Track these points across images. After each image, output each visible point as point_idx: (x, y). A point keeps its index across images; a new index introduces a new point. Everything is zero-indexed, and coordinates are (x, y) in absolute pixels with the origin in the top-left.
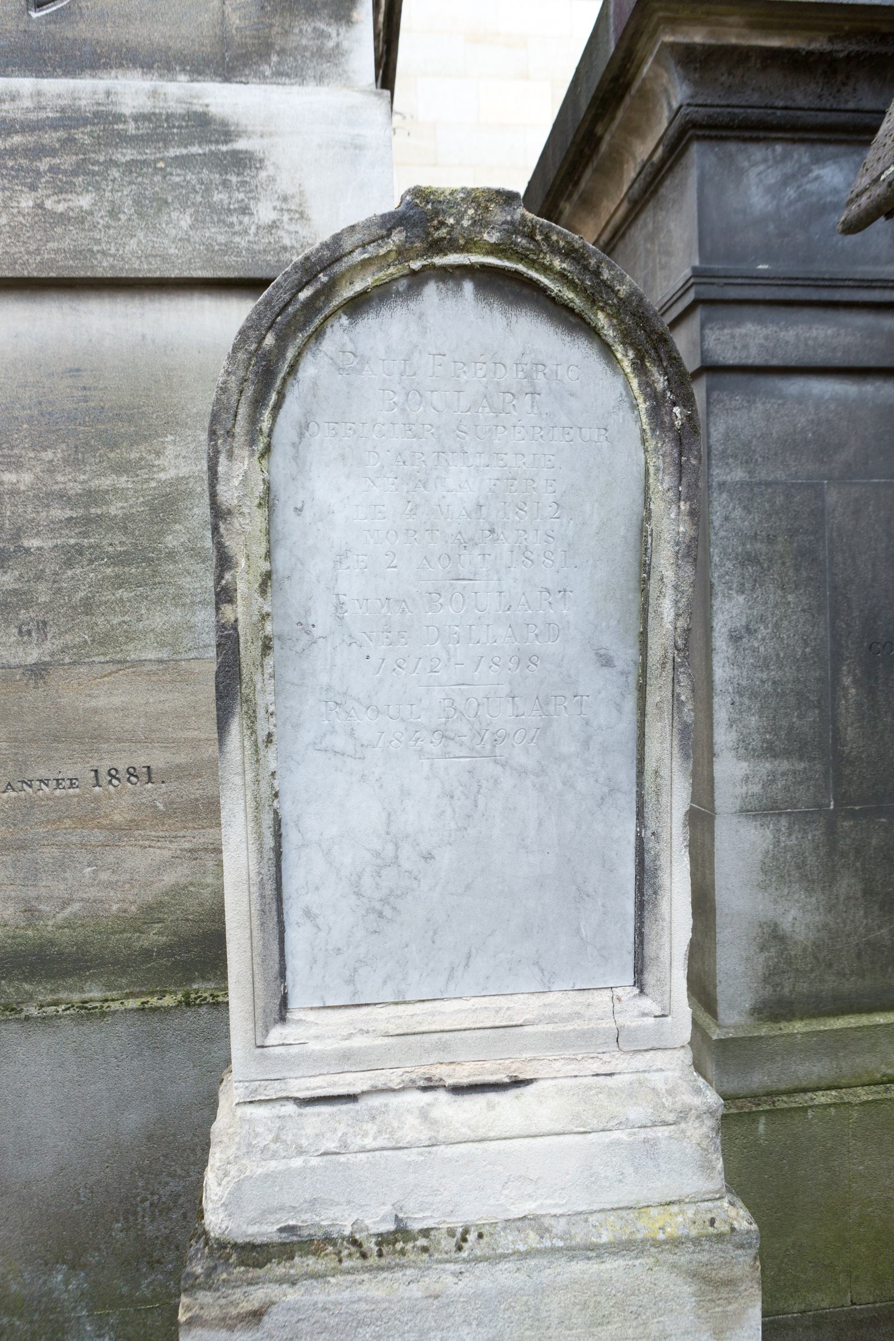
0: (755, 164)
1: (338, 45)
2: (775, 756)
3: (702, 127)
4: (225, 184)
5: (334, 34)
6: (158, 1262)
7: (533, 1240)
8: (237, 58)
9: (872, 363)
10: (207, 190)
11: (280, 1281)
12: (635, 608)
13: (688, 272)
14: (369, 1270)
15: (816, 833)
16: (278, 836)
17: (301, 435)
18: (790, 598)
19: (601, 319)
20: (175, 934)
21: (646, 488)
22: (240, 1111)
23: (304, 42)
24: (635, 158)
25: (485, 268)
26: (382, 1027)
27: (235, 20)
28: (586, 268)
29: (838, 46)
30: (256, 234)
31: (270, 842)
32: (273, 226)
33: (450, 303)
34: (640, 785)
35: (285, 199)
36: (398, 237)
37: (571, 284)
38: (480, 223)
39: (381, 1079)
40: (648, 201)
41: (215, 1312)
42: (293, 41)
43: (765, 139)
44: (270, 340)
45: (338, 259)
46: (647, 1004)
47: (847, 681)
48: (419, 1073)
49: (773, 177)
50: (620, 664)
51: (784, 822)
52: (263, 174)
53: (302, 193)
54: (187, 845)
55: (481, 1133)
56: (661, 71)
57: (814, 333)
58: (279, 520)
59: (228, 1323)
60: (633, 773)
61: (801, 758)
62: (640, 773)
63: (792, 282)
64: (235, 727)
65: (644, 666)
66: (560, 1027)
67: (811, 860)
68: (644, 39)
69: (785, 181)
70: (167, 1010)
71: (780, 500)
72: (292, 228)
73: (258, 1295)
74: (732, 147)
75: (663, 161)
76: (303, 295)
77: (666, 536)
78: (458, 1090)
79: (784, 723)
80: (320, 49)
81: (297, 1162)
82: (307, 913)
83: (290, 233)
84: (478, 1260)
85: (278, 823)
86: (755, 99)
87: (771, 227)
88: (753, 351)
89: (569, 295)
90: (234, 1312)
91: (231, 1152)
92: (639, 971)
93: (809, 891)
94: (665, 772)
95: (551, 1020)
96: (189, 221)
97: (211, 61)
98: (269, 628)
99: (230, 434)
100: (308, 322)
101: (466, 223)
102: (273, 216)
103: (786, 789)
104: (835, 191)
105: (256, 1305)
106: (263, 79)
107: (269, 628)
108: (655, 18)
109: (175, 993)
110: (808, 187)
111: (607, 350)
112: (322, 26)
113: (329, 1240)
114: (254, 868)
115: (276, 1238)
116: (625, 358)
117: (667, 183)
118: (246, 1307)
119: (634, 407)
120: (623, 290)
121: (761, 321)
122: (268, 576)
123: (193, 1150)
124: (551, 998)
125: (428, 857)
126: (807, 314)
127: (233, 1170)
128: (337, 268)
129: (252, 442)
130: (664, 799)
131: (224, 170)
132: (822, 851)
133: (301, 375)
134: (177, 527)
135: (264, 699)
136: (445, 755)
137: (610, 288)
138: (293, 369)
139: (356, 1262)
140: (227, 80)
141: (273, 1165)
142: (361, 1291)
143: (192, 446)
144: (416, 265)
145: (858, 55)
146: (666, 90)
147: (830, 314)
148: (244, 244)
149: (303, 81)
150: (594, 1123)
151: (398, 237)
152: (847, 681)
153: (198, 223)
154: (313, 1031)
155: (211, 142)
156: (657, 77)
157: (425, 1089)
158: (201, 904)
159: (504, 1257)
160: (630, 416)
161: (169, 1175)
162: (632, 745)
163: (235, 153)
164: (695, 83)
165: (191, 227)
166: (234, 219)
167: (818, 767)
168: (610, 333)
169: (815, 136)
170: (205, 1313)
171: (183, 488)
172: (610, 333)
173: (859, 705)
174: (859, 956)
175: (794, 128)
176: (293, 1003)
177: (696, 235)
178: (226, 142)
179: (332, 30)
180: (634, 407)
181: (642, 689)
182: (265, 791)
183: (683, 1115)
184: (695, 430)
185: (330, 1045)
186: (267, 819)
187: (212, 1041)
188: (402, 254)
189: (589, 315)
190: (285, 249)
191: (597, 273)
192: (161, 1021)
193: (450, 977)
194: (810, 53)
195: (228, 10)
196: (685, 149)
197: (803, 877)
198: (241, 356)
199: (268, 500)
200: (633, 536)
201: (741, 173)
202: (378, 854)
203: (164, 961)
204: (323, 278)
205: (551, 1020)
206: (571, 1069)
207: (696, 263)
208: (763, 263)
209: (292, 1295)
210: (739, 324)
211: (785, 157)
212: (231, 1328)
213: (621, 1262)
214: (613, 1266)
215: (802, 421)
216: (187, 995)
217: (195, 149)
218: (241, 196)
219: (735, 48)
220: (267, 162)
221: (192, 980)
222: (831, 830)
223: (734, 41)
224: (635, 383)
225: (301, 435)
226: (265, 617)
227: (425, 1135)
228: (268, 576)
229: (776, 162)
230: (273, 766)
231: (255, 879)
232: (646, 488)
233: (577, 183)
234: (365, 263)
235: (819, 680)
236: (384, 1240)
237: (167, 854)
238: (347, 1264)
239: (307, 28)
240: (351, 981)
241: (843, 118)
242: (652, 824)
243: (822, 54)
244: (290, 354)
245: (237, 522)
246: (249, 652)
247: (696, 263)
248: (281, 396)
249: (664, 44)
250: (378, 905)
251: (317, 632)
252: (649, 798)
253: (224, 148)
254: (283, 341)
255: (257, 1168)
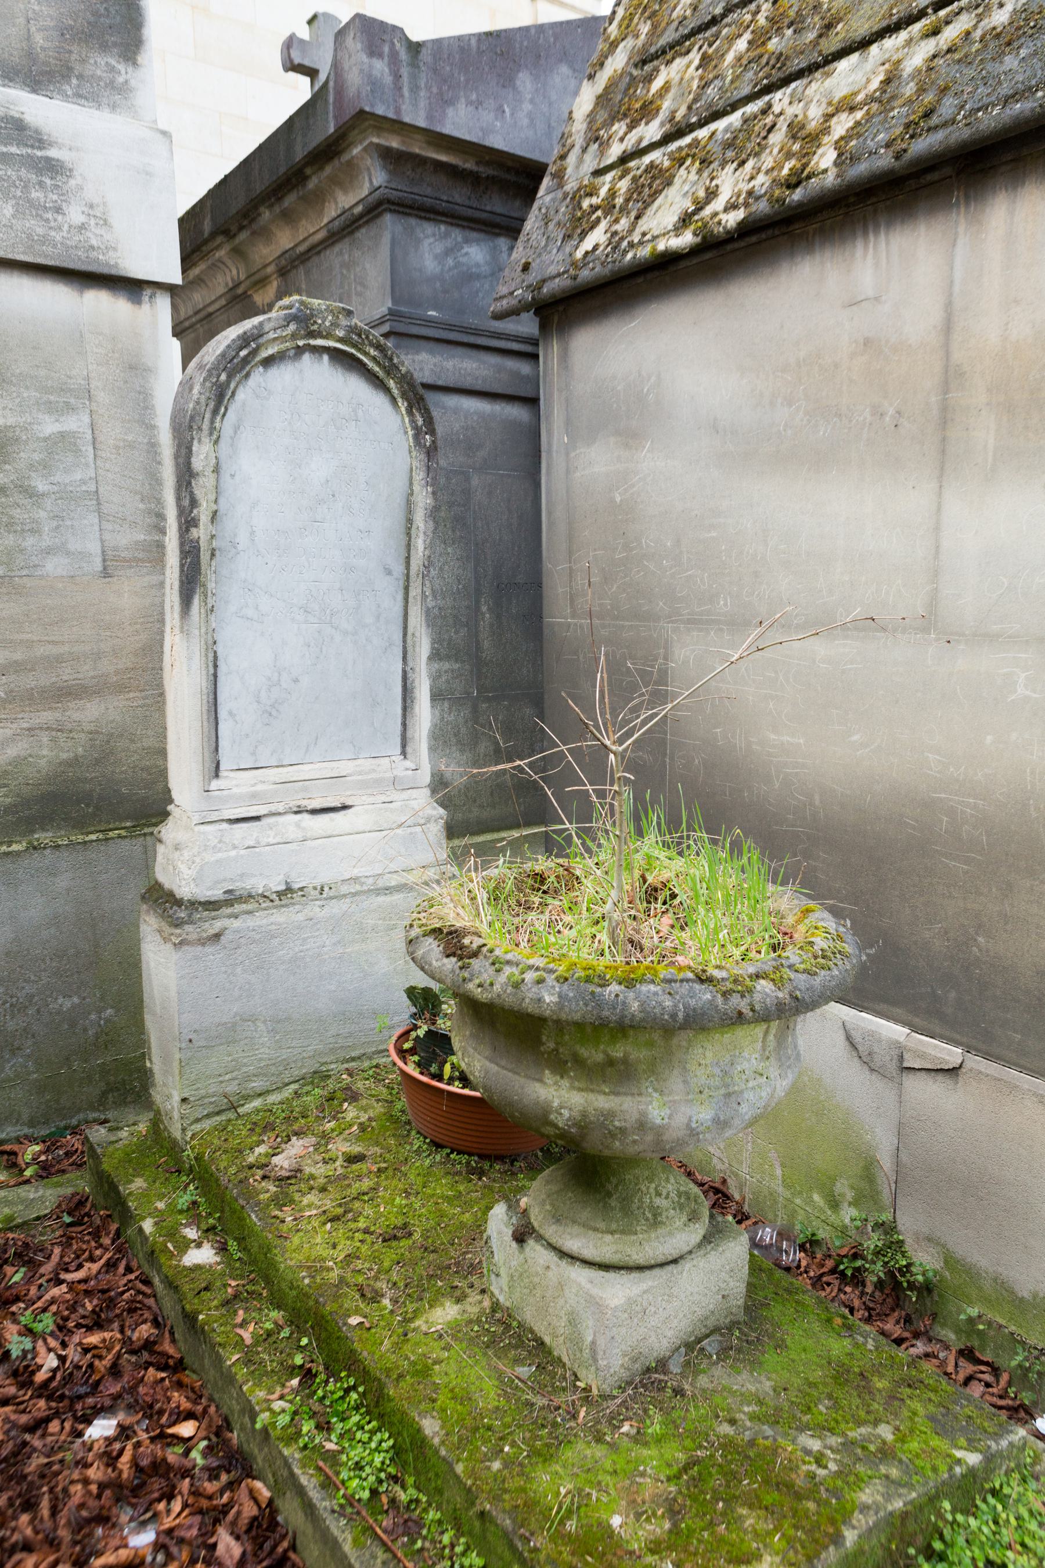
0: (427, 237)
1: (126, 81)
2: (440, 659)
3: (393, 203)
4: (41, 184)
5: (123, 71)
6: (18, 1049)
7: (358, 887)
8: (43, 73)
9: (500, 391)
10: (25, 187)
11: (229, 917)
12: (404, 543)
13: (384, 310)
14: (276, 907)
15: (466, 712)
16: (216, 666)
17: (235, 433)
18: (449, 550)
19: (392, 384)
20: (18, 795)
21: (411, 478)
22: (197, 828)
23: (99, 73)
24: (336, 203)
25: (336, 350)
26: (272, 779)
27: (39, 39)
28: (386, 356)
29: (481, 169)
30: (69, 232)
31: (212, 671)
32: (82, 227)
33: (316, 365)
34: (405, 641)
35: (91, 206)
36: (292, 327)
37: (378, 364)
38: (335, 325)
39: (273, 808)
40: (344, 237)
41: (195, 936)
42: (89, 70)
43: (434, 220)
44: (223, 377)
45: (261, 336)
46: (408, 764)
47: (484, 609)
48: (293, 804)
49: (439, 248)
50: (395, 573)
51: (446, 704)
52: (72, 182)
53: (104, 204)
54: (26, 725)
55: (329, 833)
56: (366, 156)
57: (465, 365)
58: (221, 481)
59: (202, 942)
60: (401, 635)
61: (456, 661)
62: (405, 635)
63: (451, 327)
64: (196, 601)
65: (408, 576)
66: (365, 777)
67: (463, 730)
68: (356, 131)
69: (448, 252)
70: (18, 853)
71: (443, 481)
72: (98, 231)
73: (218, 925)
74: (413, 221)
75: (361, 216)
76: (243, 353)
77: (421, 505)
78: (314, 812)
79: (446, 637)
80: (112, 82)
81: (233, 853)
82: (230, 713)
83: (96, 235)
84: (332, 898)
85: (216, 658)
86: (429, 191)
87: (438, 284)
88: (427, 373)
89: (377, 369)
90: (205, 935)
91: (195, 850)
92: (404, 746)
93: (462, 751)
94: (417, 634)
95: (360, 773)
96: (11, 211)
97: (19, 71)
98: (214, 544)
99: (200, 429)
100: (243, 368)
101: (327, 324)
102: (82, 219)
103: (447, 681)
104: (478, 265)
105: (217, 931)
106: (66, 98)
107: (214, 544)
108: (367, 123)
109: (20, 842)
110: (462, 259)
111: (394, 400)
112: (113, 62)
113: (250, 896)
114: (204, 684)
115: (222, 897)
116: (403, 405)
117: (363, 230)
118: (211, 932)
119: (406, 433)
120: (403, 370)
121: (431, 352)
122: (215, 513)
123: (43, 960)
124: (359, 762)
125: (296, 681)
126: (460, 350)
127: (197, 860)
128: (261, 341)
129: (211, 434)
130: (417, 649)
131: (40, 172)
132: (470, 724)
133: (236, 397)
134: (7, 467)
135: (211, 585)
136: (306, 622)
137: (397, 368)
138: (233, 393)
139: (268, 904)
140: (34, 91)
141: (220, 855)
142: (272, 919)
143: (17, 400)
144: (301, 343)
145: (493, 177)
146: (368, 169)
147: (474, 353)
148: (58, 238)
149: (99, 107)
150: (385, 826)
151: (292, 327)
152: (484, 609)
153: (18, 213)
154: (234, 782)
155: (27, 145)
156: (362, 158)
157: (296, 813)
158: (39, 772)
159: (344, 896)
160: (404, 438)
161: (25, 981)
162: (401, 619)
163: (48, 160)
164: (390, 172)
165: (14, 216)
166: (49, 216)
167: (467, 667)
168: (395, 392)
169: (465, 224)
170: (189, 937)
171: (11, 435)
172: (395, 392)
173: (491, 625)
174: (492, 794)
175: (453, 216)
176: (222, 767)
177: (389, 283)
178: (40, 148)
179: (121, 67)
180: (406, 433)
181: (407, 589)
182: (210, 642)
183: (428, 820)
184: (436, 448)
185: (244, 790)
186: (211, 655)
187: (55, 875)
188: (294, 336)
189: (386, 381)
190: (92, 247)
191: (391, 359)
192: (13, 863)
193: (307, 750)
194: (464, 170)
195: (33, 29)
196: (380, 215)
197: (459, 742)
198: (208, 384)
199: (217, 470)
200: (403, 503)
201: (419, 241)
202: (269, 679)
203: (10, 818)
204: (253, 345)
205: (360, 773)
206: (371, 799)
207: (390, 305)
208: (434, 309)
209: (236, 924)
210: (417, 353)
211: (446, 236)
212: (203, 944)
213: (402, 895)
214: (397, 897)
215: (457, 426)
216: (30, 843)
217: (13, 149)
218: (55, 197)
219: (417, 156)
220: (75, 173)
221: (33, 832)
222: (475, 710)
223: (417, 151)
224: (407, 420)
225: (235, 433)
226: (213, 537)
227: (300, 836)
228: (215, 513)
229: (441, 238)
230: (214, 625)
231: (205, 691)
232: (411, 478)
233: (280, 199)
234: (275, 339)
235: (467, 607)
236: (280, 894)
237: (9, 732)
238: (264, 905)
239: (102, 60)
240: (254, 754)
241: (484, 215)
242: (411, 664)
243: (471, 172)
244: (232, 385)
245: (201, 480)
246: (204, 556)
247: (390, 305)
248: (226, 409)
249: (371, 143)
250: (269, 709)
251: (240, 547)
252: (410, 649)
253: (39, 153)
254: (230, 377)
255: (210, 857)
